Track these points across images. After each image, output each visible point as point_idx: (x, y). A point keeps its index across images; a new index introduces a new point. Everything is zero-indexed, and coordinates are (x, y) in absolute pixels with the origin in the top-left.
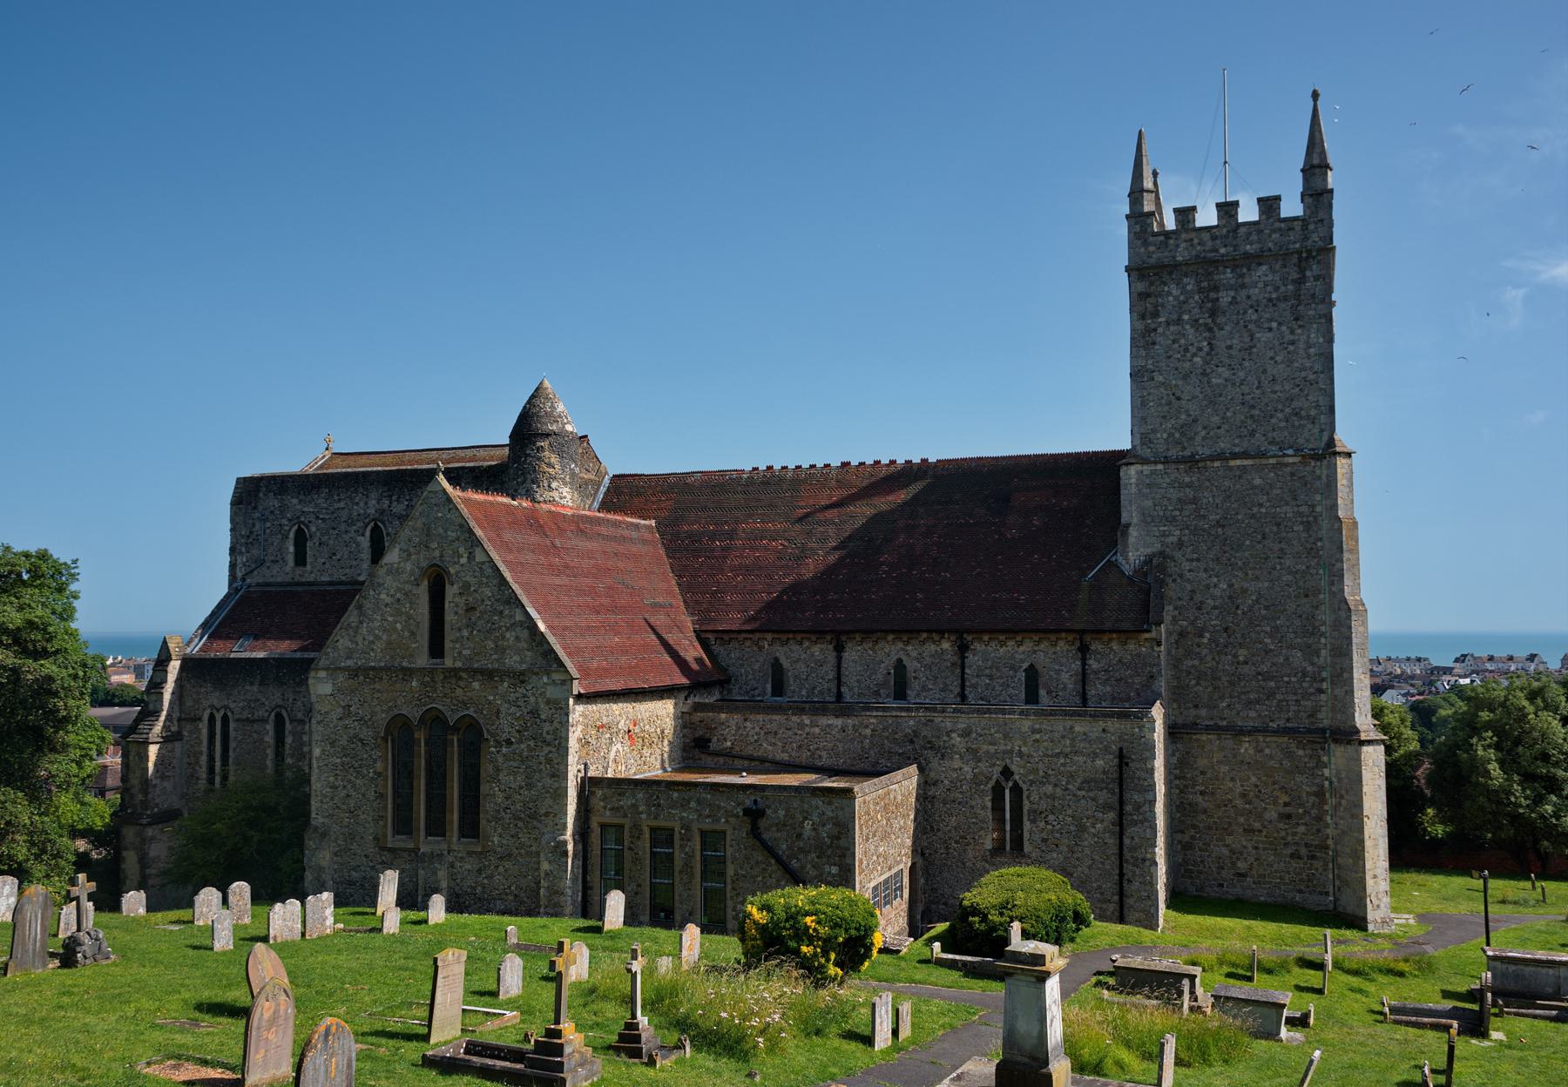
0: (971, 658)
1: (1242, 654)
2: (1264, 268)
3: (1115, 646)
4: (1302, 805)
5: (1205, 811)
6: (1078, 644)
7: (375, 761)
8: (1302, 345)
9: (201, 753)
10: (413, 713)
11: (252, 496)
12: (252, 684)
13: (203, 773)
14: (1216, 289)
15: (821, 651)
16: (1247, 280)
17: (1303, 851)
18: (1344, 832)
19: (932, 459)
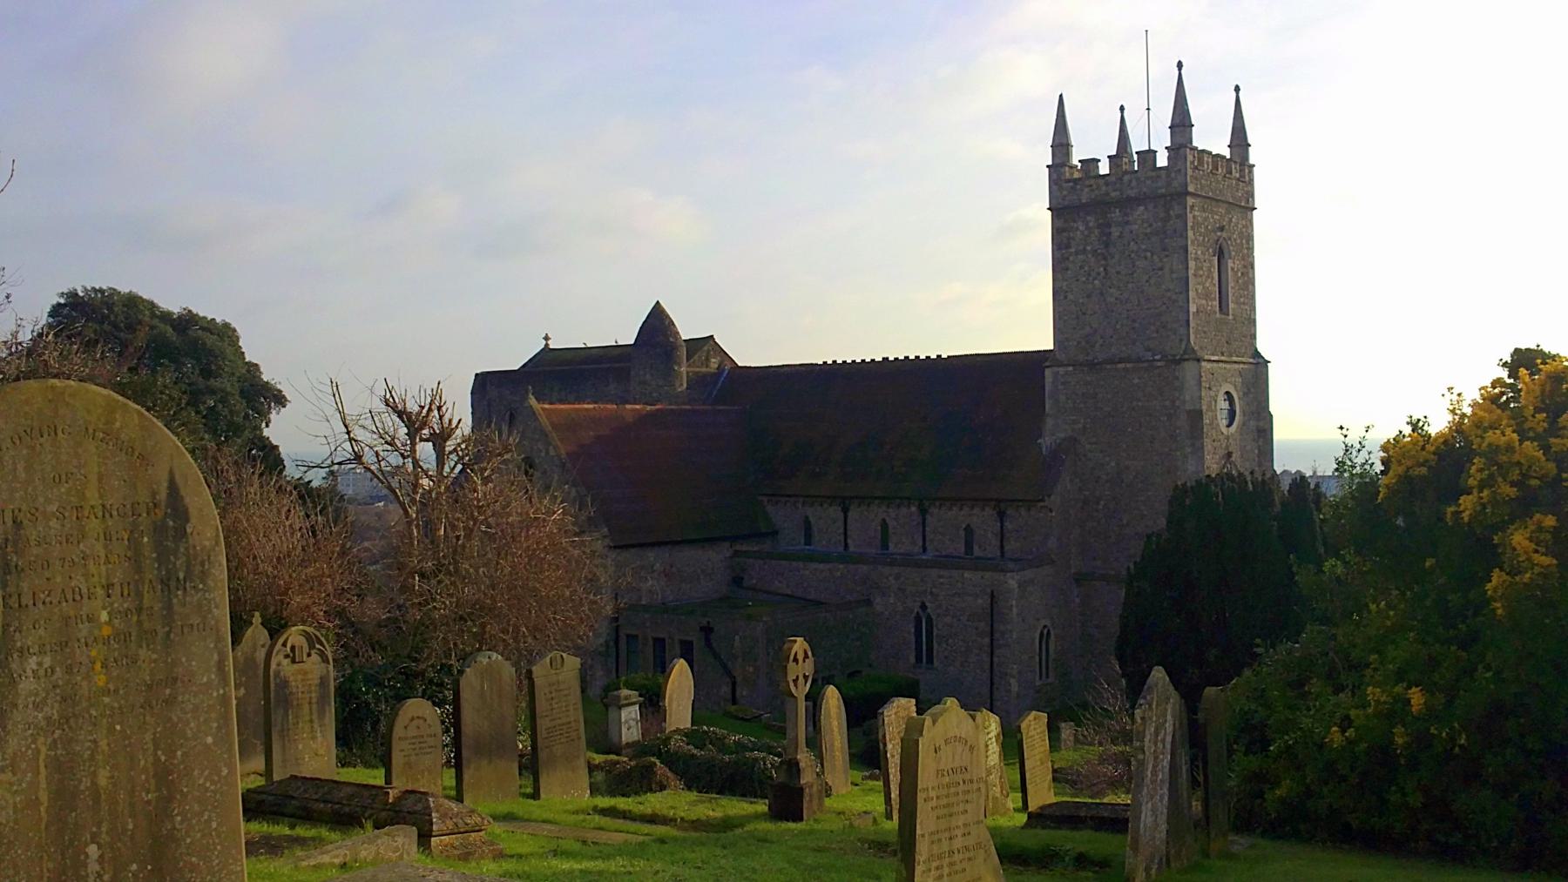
3: (1023, 511)
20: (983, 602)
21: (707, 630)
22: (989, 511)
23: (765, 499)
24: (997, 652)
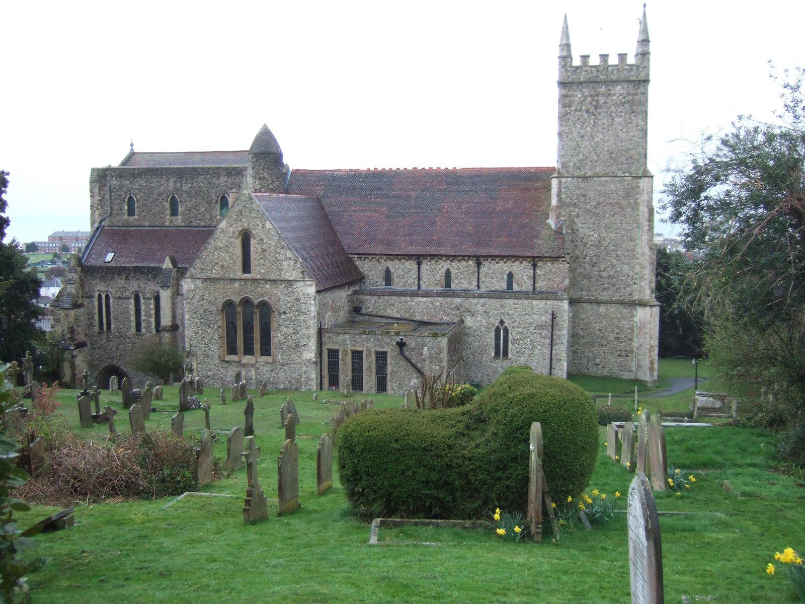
0: (483, 269)
1: (603, 267)
2: (620, 87)
4: (624, 334)
5: (583, 337)
6: (532, 263)
7: (217, 321)
8: (634, 125)
9: (95, 314)
10: (237, 299)
11: (101, 177)
12: (121, 279)
13: (96, 323)
14: (598, 95)
15: (411, 265)
16: (612, 92)
17: (624, 353)
18: (641, 345)
19: (458, 168)
20: (546, 318)
21: (401, 345)
22: (525, 264)
23: (356, 257)
24: (554, 347)
